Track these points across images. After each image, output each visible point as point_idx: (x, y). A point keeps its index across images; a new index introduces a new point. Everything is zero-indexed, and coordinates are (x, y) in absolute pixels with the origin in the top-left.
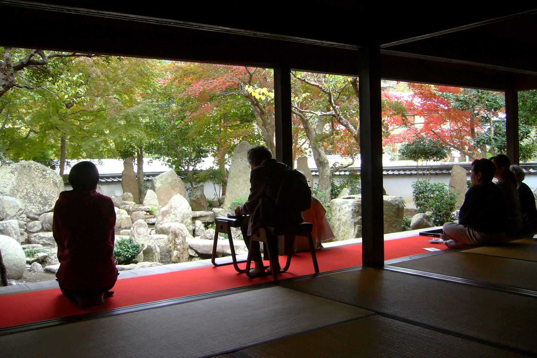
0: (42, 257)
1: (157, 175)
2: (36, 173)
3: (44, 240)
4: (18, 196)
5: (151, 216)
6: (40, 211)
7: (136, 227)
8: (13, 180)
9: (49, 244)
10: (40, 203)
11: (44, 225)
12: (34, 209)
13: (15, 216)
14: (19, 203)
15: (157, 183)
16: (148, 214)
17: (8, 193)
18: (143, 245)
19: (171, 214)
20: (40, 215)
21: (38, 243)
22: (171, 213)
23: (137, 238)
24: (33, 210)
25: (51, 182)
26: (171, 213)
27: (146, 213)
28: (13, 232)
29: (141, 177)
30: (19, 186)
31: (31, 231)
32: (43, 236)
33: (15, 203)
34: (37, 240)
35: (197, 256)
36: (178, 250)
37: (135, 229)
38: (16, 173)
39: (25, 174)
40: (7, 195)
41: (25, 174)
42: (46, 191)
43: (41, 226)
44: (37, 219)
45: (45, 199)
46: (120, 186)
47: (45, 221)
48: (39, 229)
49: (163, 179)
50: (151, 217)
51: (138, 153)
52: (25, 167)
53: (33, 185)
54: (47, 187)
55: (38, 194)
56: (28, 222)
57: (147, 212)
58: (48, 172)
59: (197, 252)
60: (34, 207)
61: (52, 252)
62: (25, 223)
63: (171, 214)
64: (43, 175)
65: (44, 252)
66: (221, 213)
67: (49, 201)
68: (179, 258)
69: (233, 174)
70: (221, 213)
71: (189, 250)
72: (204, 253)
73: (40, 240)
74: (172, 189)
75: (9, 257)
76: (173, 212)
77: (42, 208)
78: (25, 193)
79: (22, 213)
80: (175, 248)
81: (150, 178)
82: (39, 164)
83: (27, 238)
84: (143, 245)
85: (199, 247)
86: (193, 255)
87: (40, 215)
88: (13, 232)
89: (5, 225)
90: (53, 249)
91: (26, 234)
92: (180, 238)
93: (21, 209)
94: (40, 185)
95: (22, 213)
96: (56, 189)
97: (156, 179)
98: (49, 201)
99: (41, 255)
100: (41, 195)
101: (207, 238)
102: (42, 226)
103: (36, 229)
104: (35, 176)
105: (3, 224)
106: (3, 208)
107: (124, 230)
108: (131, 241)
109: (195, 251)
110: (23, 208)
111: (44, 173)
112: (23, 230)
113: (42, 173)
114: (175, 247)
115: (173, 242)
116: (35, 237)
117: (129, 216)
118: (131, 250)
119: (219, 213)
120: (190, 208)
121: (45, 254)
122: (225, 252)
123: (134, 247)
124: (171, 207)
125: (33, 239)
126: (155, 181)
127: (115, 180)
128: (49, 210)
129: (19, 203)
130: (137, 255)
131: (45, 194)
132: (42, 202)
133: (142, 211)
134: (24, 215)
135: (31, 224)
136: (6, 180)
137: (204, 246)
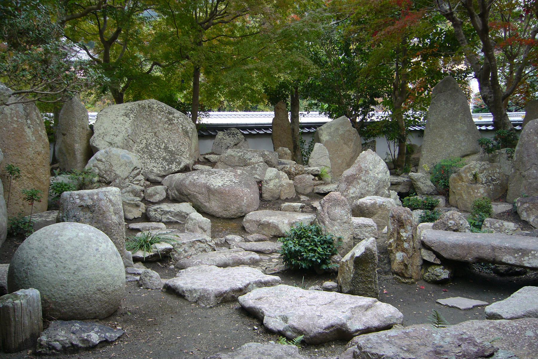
0: (163, 251)
1: (319, 126)
2: (160, 117)
3: (168, 216)
4: (134, 148)
5: (321, 182)
6: (165, 171)
7: (327, 205)
8: (127, 125)
9: (177, 223)
10: (164, 159)
11: (169, 191)
12: (155, 168)
13: (128, 177)
14: (134, 158)
15: (324, 135)
16: (317, 178)
17: (120, 144)
18: (340, 239)
19: (360, 181)
20: (164, 176)
21: (160, 221)
22: (360, 178)
23: (330, 226)
24: (155, 170)
25: (180, 130)
26: (360, 178)
27: (313, 177)
28: (112, 209)
29: (296, 128)
30: (136, 134)
31: (151, 200)
32: (168, 209)
33: (128, 158)
34: (158, 216)
35: (439, 262)
36: (404, 250)
37: (325, 210)
38: (132, 115)
39: (144, 118)
40: (118, 147)
41: (144, 118)
42: (173, 142)
43: (165, 194)
44: (160, 183)
45: (172, 153)
46: (270, 140)
47: (171, 186)
48: (162, 198)
49: (332, 129)
50: (321, 184)
51: (292, 96)
52: (144, 108)
53: (156, 133)
54: (174, 137)
55: (163, 147)
56: (147, 187)
57: (315, 175)
58: (175, 115)
59: (438, 255)
60: (155, 165)
61: (180, 242)
62: (143, 188)
63: (360, 181)
64: (169, 120)
65: (166, 240)
66: (422, 180)
67: (177, 156)
68: (406, 266)
69: (433, 123)
70: (422, 180)
71: (423, 250)
72: (455, 258)
73: (163, 216)
74: (345, 144)
75: (86, 273)
76: (363, 178)
77: (167, 167)
78: (144, 145)
79: (138, 174)
80: (399, 247)
81: (311, 131)
82: (163, 105)
83: (144, 211)
84: (340, 239)
85: (445, 246)
86: (432, 261)
87: (164, 176)
88: (112, 209)
89: (95, 197)
90: (180, 235)
91: (143, 205)
92: (409, 228)
93: (135, 168)
94: (164, 134)
95: (138, 174)
96: (187, 140)
97: (321, 129)
98: (177, 156)
99: (162, 246)
100: (166, 148)
101: (448, 229)
102: (167, 194)
103: (157, 198)
104: (158, 121)
105: (93, 194)
106: (111, 165)
107: (287, 204)
108: (318, 232)
109: (435, 252)
110: (139, 166)
111: (171, 116)
112: (138, 199)
113: (167, 117)
114: (398, 245)
115: (396, 235)
116: (156, 210)
117: (291, 182)
118: (320, 249)
119: (418, 179)
120: (388, 172)
121: (168, 246)
122: (498, 259)
123: (325, 242)
124: (360, 170)
125: (152, 214)
126: (321, 132)
127: (261, 132)
128: (176, 170)
129: (134, 158)
130: (330, 259)
131: (171, 147)
132: (167, 157)
133: (308, 174)
134: (141, 177)
135: (150, 190)
136: (117, 126)
137: (455, 246)
